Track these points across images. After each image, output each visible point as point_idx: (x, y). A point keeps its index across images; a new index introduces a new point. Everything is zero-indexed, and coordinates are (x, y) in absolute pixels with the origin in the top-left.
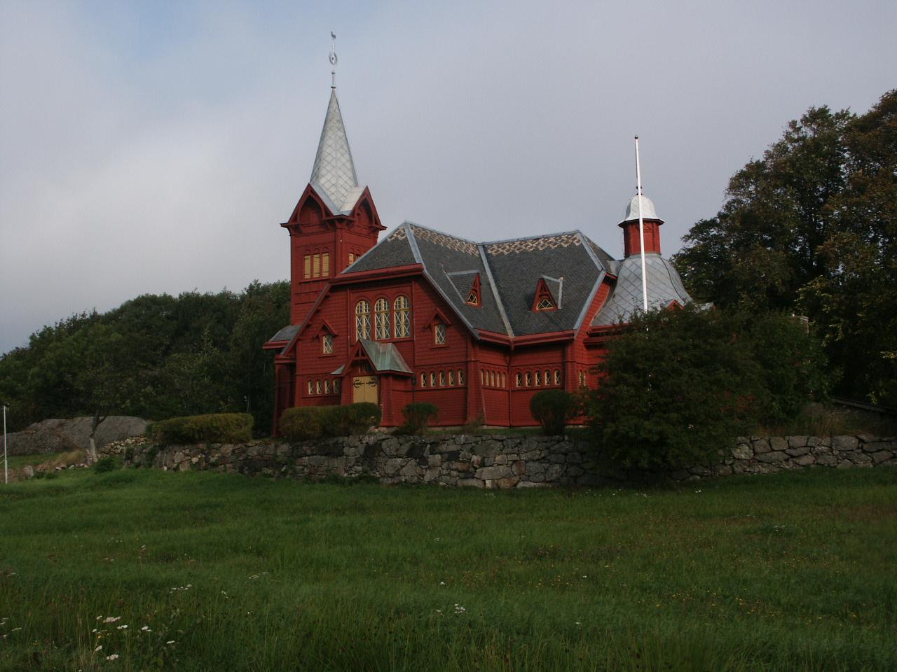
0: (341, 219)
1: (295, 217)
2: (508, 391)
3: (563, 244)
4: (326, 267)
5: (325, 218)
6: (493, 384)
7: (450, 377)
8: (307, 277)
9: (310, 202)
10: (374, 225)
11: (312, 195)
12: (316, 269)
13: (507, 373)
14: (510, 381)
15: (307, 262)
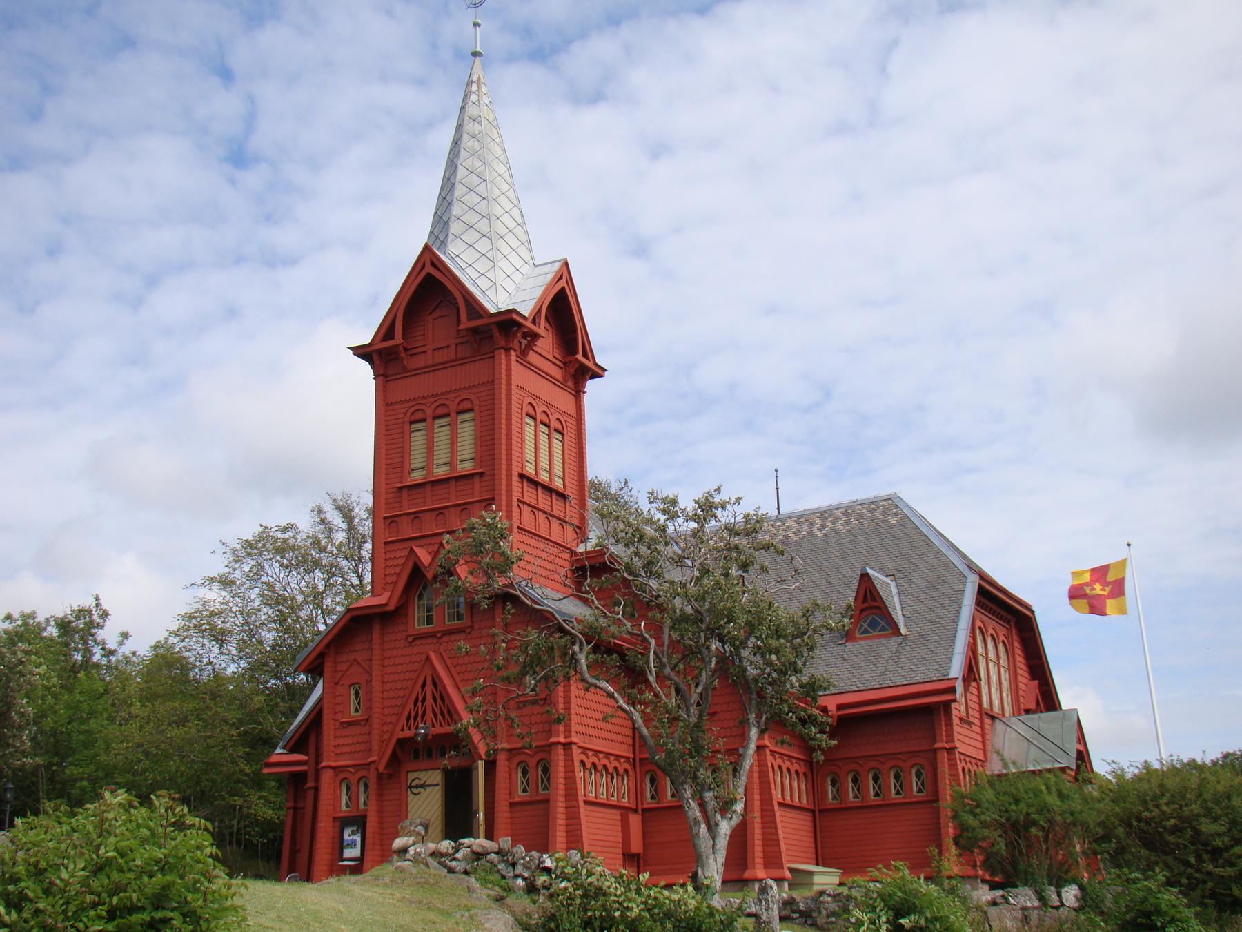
0: (508, 323)
1: (387, 330)
2: (813, 812)
5: (465, 323)
6: (788, 797)
8: (417, 477)
9: (431, 291)
10: (580, 357)
13: (631, 772)
15: (417, 440)
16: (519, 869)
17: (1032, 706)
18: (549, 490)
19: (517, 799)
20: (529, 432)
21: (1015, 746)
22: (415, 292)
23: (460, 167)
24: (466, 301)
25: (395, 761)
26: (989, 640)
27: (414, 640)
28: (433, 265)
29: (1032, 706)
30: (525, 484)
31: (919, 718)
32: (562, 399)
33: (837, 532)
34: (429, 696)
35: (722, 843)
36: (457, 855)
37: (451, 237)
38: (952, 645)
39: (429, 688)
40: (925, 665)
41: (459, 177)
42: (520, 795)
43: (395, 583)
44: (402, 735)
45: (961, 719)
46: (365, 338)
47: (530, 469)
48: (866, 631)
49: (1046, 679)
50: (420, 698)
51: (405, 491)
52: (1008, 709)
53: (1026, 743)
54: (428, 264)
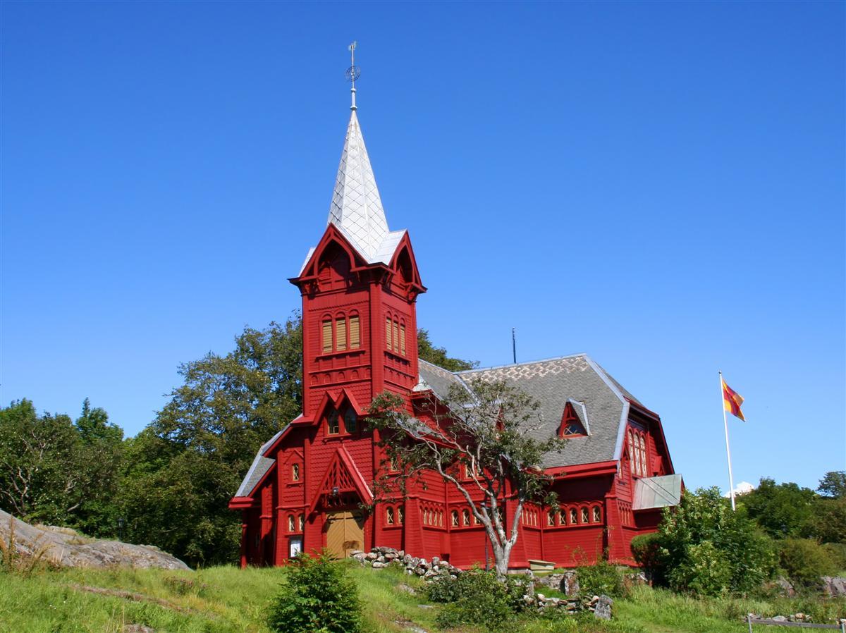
0: (378, 269)
3: (526, 375)
4: (355, 337)
7: (290, 523)
8: (327, 351)
11: (336, 239)
12: (341, 340)
14: (542, 520)
16: (409, 566)
17: (658, 471)
18: (399, 359)
19: (387, 527)
20: (388, 327)
21: (650, 494)
22: (326, 248)
23: (347, 176)
24: (355, 257)
25: (320, 508)
26: (635, 436)
27: (328, 441)
28: (335, 235)
29: (658, 471)
30: (387, 357)
31: (592, 486)
32: (403, 306)
33: (552, 374)
34: (338, 472)
35: (507, 554)
36: (378, 559)
37: (343, 217)
38: (615, 442)
39: (338, 466)
40: (601, 453)
41: (346, 182)
42: (388, 524)
43: (318, 409)
44: (323, 492)
45: (619, 482)
46: (298, 274)
47: (389, 347)
48: (569, 433)
49: (666, 455)
50: (333, 473)
51: (321, 361)
52: (645, 472)
53: (654, 493)
54: (332, 234)
